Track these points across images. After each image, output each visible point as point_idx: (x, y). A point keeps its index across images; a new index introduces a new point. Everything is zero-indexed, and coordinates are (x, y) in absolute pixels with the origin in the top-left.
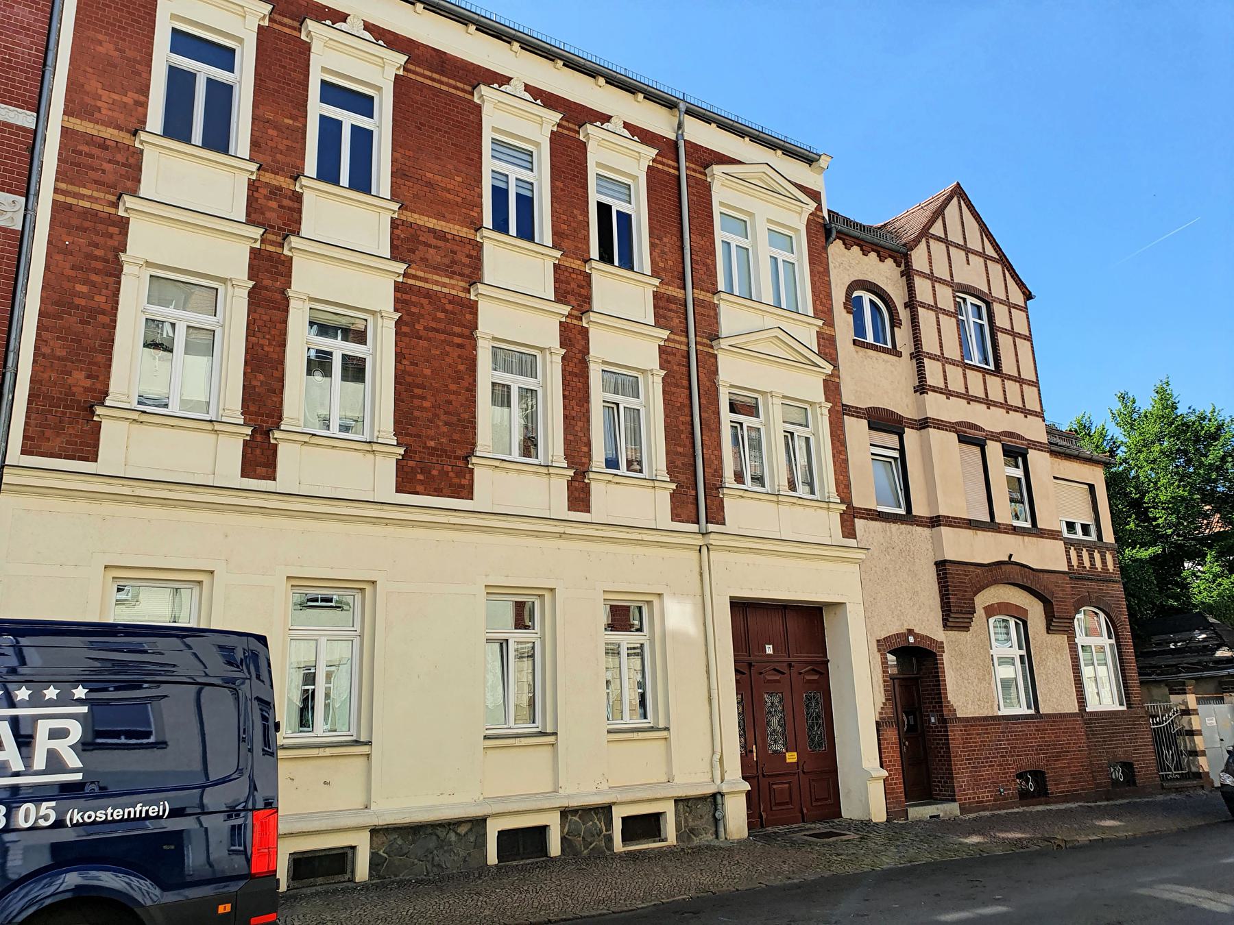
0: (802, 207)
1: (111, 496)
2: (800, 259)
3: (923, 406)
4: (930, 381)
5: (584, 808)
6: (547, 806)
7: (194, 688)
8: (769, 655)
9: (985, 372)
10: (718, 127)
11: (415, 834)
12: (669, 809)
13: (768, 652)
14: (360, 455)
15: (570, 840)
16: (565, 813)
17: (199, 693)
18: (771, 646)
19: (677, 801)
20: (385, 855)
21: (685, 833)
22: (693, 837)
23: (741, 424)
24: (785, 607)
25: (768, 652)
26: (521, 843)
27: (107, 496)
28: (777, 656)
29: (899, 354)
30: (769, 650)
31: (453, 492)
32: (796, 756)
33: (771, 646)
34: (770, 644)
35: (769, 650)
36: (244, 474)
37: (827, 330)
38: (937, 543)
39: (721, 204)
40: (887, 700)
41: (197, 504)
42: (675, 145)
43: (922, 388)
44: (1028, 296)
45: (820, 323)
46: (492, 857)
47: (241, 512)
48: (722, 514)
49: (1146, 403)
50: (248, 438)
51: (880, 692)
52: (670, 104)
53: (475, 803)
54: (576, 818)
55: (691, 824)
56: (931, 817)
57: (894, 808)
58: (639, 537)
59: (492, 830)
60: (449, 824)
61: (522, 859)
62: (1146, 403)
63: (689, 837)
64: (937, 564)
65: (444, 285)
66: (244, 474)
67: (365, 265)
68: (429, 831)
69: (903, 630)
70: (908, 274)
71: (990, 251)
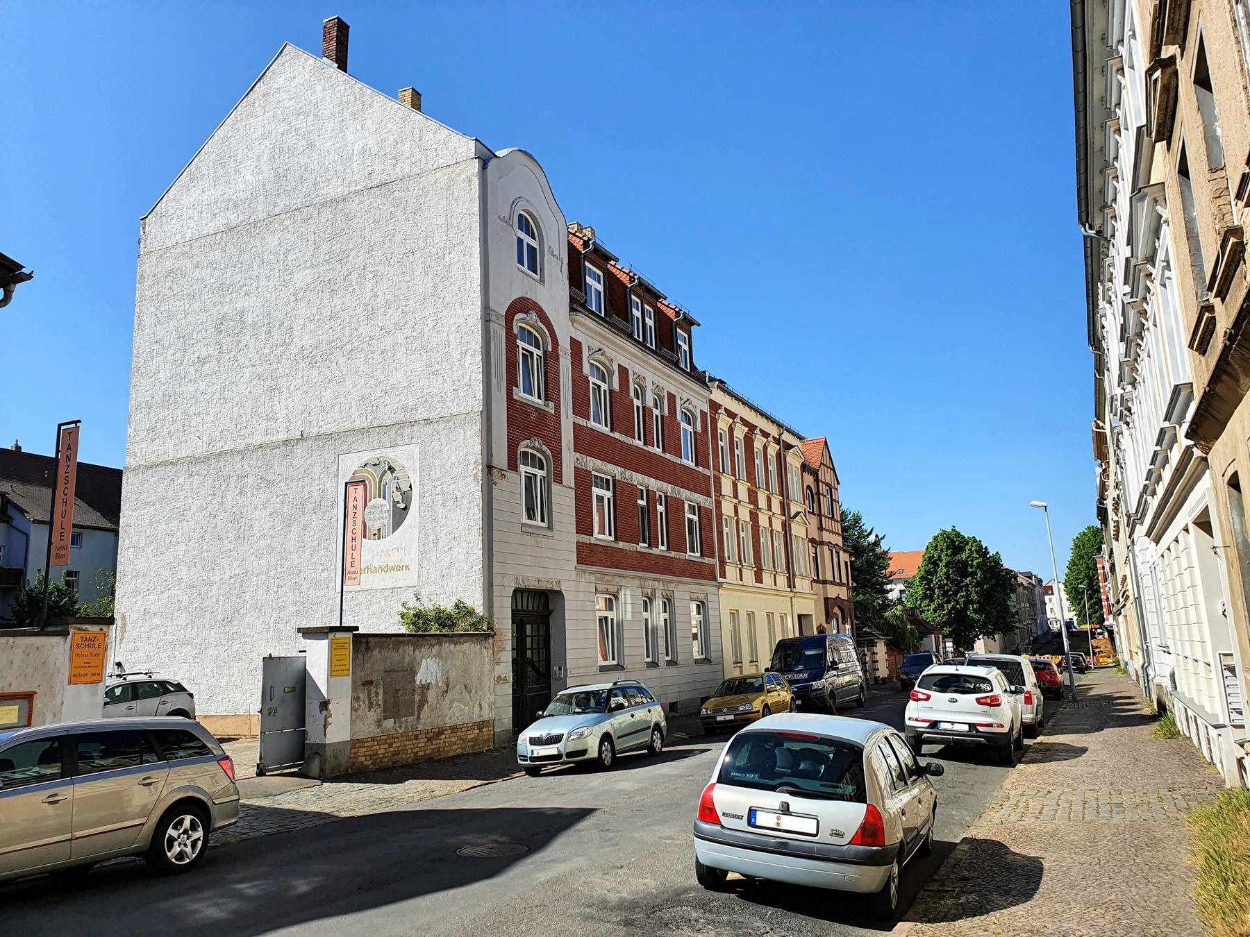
2: (741, 453)
3: (821, 536)
4: (824, 526)
7: (48, 519)
9: (829, 518)
17: (44, 522)
23: (535, 476)
29: (814, 514)
37: (752, 488)
38: (825, 590)
39: (720, 429)
42: (779, 439)
43: (821, 529)
44: (838, 483)
45: (749, 485)
49: (884, 546)
52: (779, 425)
62: (884, 546)
64: (825, 598)
70: (817, 480)
71: (831, 467)
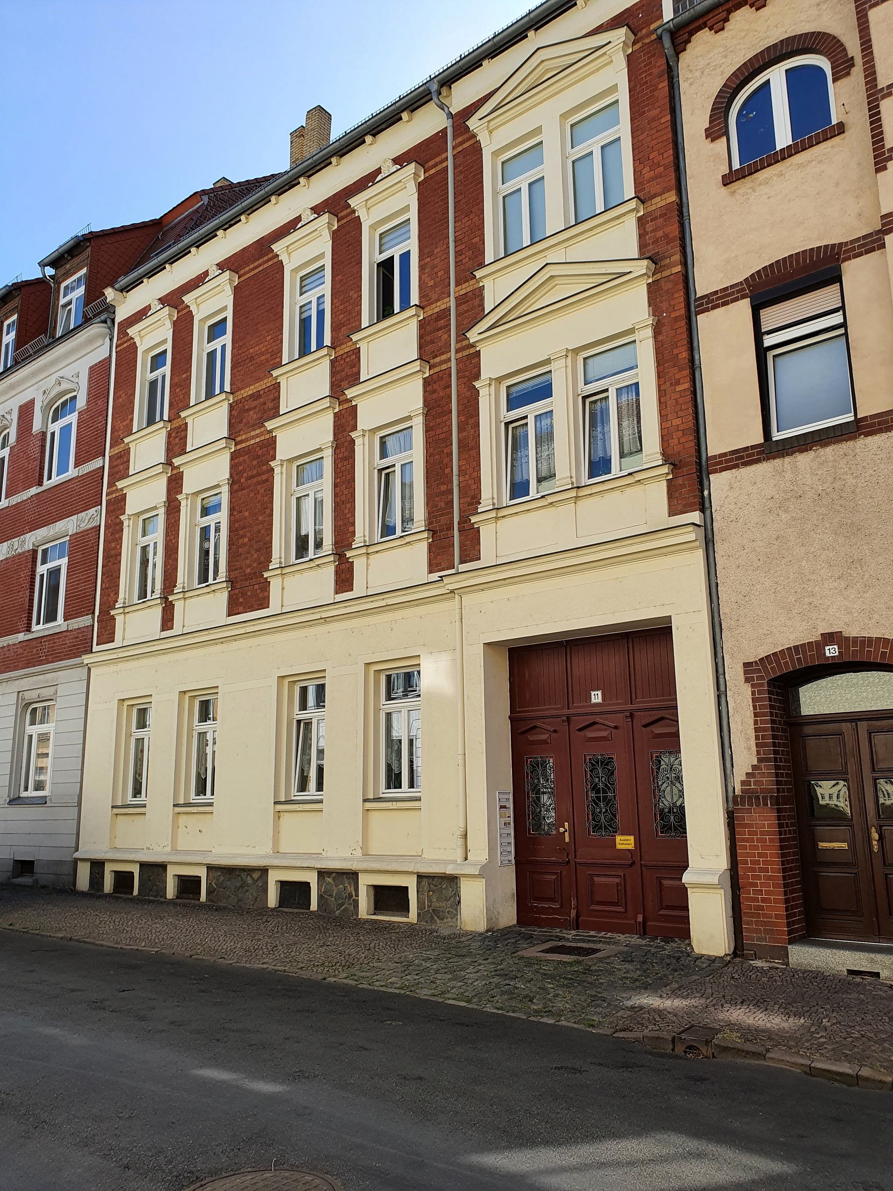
0: (605, 53)
1: (495, 584)
2: (313, 295)
5: (337, 871)
6: (299, 865)
8: (597, 705)
10: (492, 58)
11: (230, 874)
12: (411, 883)
13: (593, 701)
14: (617, 493)
15: (327, 899)
16: (420, 877)
18: (599, 693)
19: (420, 877)
20: (215, 886)
21: (427, 913)
22: (436, 918)
24: (627, 635)
25: (593, 701)
26: (297, 895)
27: (268, 631)
28: (609, 705)
30: (597, 697)
31: (259, 605)
32: (632, 841)
33: (599, 693)
34: (598, 690)
35: (597, 697)
36: (672, 513)
40: (760, 760)
41: (366, 612)
46: (272, 899)
47: (673, 552)
48: (477, 548)
50: (671, 477)
51: (749, 749)
53: (263, 857)
54: (329, 880)
55: (436, 904)
56: (851, 972)
57: (759, 939)
58: (383, 603)
59: (274, 878)
60: (249, 870)
61: (296, 908)
63: (432, 918)
65: (257, 436)
66: (672, 513)
67: (363, 393)
68: (237, 873)
69: (815, 637)
